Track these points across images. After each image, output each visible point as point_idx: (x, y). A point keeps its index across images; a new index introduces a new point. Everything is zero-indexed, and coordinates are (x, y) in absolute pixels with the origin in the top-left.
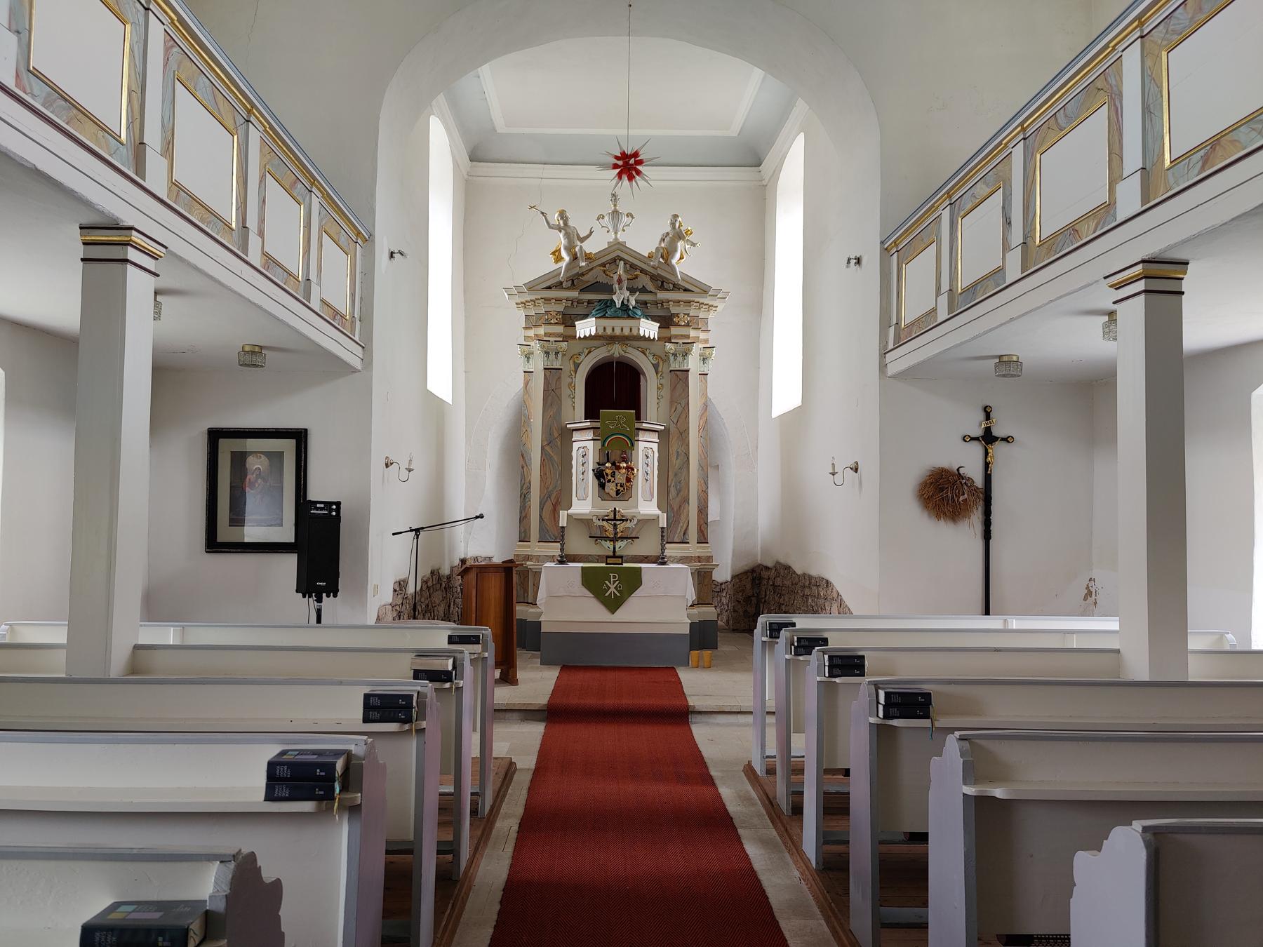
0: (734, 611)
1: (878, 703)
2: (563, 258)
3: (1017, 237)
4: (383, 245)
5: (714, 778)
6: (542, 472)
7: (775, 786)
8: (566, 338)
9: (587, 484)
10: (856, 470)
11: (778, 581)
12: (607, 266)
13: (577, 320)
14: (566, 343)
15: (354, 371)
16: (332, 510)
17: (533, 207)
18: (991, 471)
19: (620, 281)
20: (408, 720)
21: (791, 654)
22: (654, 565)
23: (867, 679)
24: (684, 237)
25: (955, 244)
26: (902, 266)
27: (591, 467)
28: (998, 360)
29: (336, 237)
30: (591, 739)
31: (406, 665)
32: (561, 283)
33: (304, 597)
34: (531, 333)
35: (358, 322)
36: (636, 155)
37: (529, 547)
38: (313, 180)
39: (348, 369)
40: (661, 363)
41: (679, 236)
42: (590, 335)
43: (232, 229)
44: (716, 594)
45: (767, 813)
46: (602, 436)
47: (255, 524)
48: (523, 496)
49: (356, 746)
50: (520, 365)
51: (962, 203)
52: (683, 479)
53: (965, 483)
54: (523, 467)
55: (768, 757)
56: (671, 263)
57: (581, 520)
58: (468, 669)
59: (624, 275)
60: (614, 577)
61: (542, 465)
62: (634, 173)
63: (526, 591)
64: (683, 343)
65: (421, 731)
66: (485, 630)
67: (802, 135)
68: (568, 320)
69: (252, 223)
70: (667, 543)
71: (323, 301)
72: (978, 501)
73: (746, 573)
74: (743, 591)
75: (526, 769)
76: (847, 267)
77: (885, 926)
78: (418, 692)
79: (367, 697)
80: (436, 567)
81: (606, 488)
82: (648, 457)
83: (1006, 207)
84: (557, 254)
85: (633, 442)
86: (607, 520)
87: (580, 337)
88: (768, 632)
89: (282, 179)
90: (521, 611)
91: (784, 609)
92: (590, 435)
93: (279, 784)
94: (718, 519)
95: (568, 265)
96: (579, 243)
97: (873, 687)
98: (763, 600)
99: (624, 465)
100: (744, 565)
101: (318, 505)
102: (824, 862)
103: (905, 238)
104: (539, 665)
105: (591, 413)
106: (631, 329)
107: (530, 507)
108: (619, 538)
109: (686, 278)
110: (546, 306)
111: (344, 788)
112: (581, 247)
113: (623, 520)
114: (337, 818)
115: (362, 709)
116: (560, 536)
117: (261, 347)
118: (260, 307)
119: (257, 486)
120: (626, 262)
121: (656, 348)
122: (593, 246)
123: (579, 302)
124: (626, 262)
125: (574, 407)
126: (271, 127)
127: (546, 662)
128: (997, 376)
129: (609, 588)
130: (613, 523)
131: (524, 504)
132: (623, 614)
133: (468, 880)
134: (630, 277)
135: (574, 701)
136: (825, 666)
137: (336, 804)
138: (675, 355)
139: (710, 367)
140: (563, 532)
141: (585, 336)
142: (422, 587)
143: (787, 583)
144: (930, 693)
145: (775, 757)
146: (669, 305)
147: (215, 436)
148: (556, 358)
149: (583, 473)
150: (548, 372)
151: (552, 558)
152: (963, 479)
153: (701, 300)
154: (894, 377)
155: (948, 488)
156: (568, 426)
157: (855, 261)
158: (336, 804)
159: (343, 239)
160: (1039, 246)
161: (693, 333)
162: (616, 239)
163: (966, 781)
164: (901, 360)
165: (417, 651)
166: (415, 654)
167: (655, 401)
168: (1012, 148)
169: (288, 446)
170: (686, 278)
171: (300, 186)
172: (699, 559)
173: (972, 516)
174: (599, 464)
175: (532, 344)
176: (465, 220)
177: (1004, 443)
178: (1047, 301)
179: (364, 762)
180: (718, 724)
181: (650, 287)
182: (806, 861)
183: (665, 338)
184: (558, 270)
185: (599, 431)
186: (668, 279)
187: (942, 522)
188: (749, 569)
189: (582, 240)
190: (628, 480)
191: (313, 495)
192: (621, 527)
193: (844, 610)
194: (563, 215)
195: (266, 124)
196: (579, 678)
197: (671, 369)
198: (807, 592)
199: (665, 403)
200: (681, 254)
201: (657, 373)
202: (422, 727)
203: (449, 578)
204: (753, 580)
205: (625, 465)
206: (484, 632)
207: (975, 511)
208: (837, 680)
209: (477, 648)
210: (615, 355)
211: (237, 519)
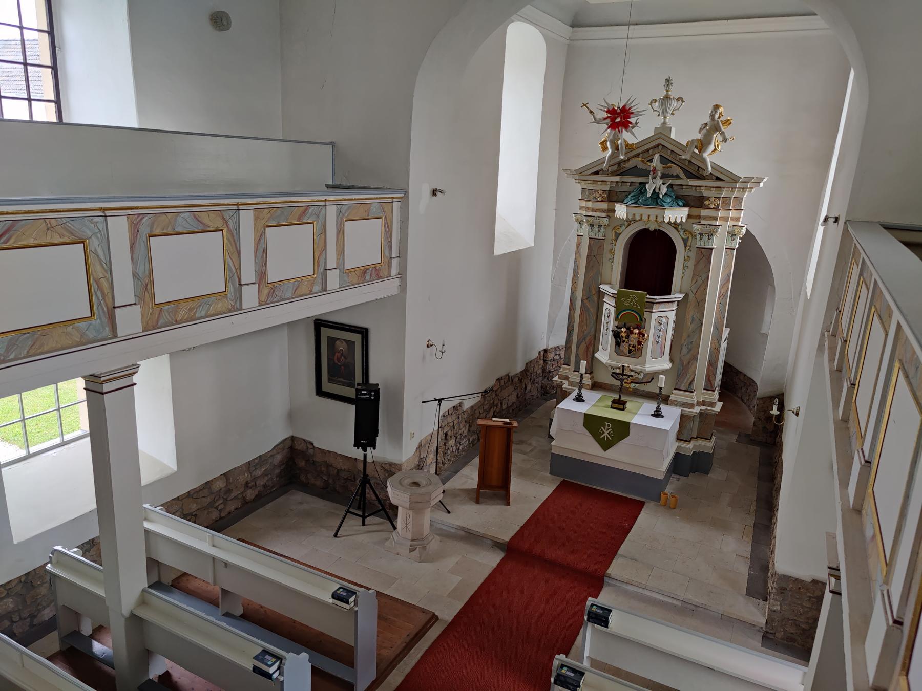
9: (608, 338)
10: (797, 414)
16: (371, 395)
27: (611, 329)
48: (569, 332)
52: (694, 340)
61: (581, 314)
81: (621, 347)
95: (610, 157)
99: (636, 331)
131: (570, 338)
138: (701, 234)
149: (607, 330)
167: (681, 271)
170: (715, 167)
174: (617, 327)
176: (565, 81)
184: (601, 161)
190: (640, 343)
199: (689, 273)
201: (686, 246)
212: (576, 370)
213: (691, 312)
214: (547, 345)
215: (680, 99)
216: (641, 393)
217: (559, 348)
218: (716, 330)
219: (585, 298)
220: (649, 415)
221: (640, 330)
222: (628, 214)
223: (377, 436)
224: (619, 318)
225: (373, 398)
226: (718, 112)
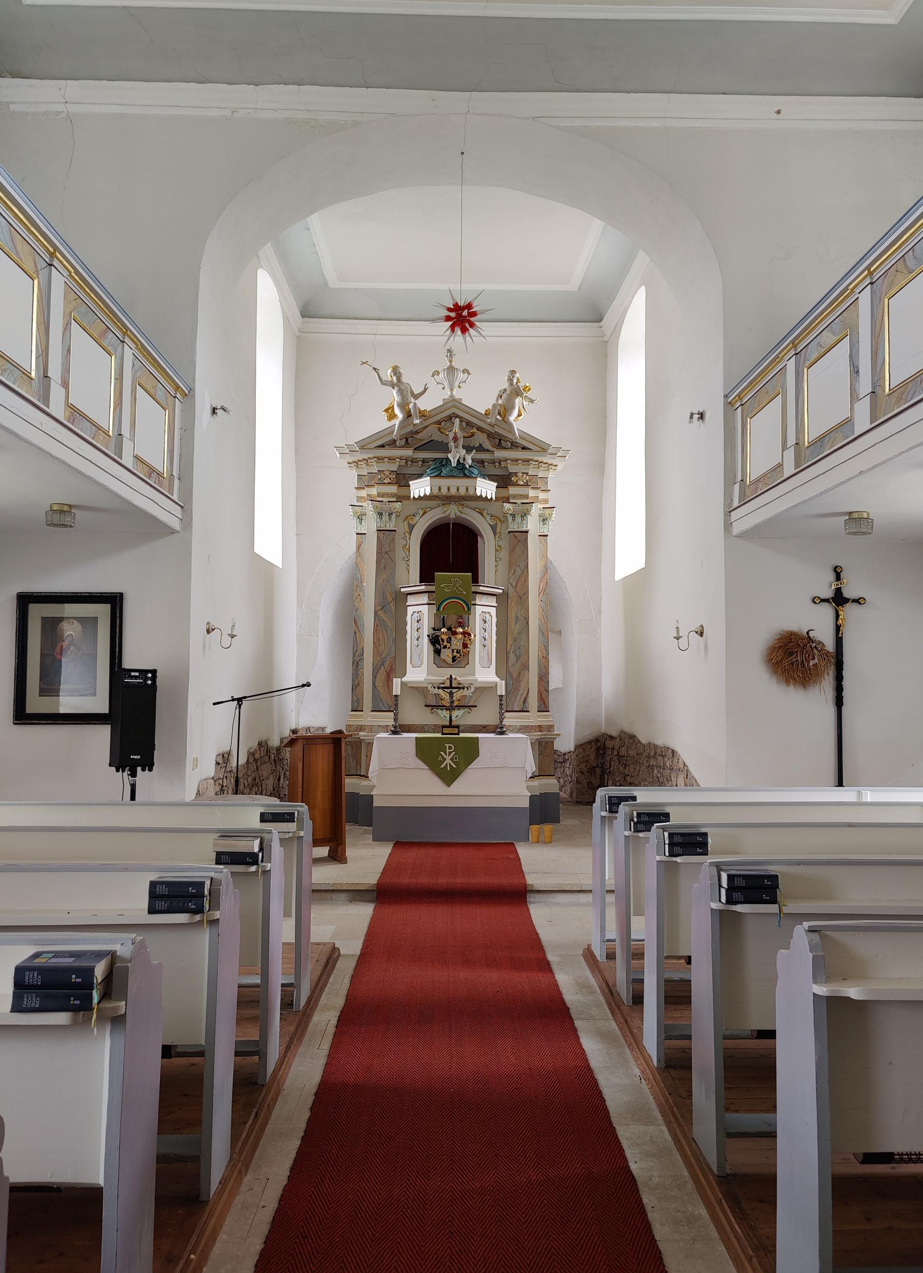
0: (578, 782)
1: (720, 886)
2: (397, 415)
3: (865, 385)
4: (204, 400)
5: (550, 963)
6: (375, 637)
7: (615, 974)
8: (400, 498)
10: (701, 634)
11: (623, 751)
12: (443, 423)
13: (411, 480)
14: (400, 503)
15: (173, 532)
16: (147, 679)
17: (365, 363)
18: (842, 634)
19: (455, 439)
20: (199, 910)
21: (630, 830)
22: (492, 735)
23: (709, 859)
24: (523, 394)
25: (801, 395)
26: (747, 420)
27: (426, 633)
28: (847, 517)
29: (152, 392)
30: (422, 921)
31: (208, 847)
32: (394, 441)
33: (118, 771)
34: (363, 493)
35: (176, 481)
36: (469, 306)
37: (362, 716)
38: (126, 331)
39: (166, 530)
40: (499, 524)
41: (517, 392)
42: (425, 495)
43: (31, 379)
44: (559, 764)
45: (607, 1001)
46: (438, 602)
47: (67, 694)
48: (355, 663)
49: (121, 945)
50: (353, 526)
51: (808, 353)
53: (815, 647)
54: (355, 633)
55: (608, 941)
56: (508, 419)
57: (416, 688)
58: (277, 850)
59: (460, 433)
60: (450, 748)
62: (467, 325)
63: (358, 763)
64: (522, 503)
65: (214, 922)
66: (301, 806)
67: (643, 288)
68: (402, 480)
69: (55, 371)
70: (507, 711)
71: (137, 458)
72: (829, 665)
74: (587, 761)
75: (350, 955)
76: (690, 422)
77: (730, 1135)
78: (212, 879)
79: (153, 885)
80: (264, 738)
83: (854, 355)
84: (390, 411)
85: (469, 606)
86: (443, 688)
87: (414, 497)
88: (607, 806)
89: (90, 328)
90: (350, 784)
91: (629, 780)
92: (424, 599)
93: (28, 993)
94: (561, 686)
95: (401, 423)
96: (413, 400)
97: (714, 869)
98: (608, 771)
100: (588, 734)
101: (133, 674)
102: (666, 1060)
103: (748, 392)
104: (371, 842)
105: (426, 576)
106: (467, 488)
107: (363, 674)
108: (456, 706)
109: (524, 435)
110: (379, 465)
111: (106, 995)
112: (415, 404)
113: (460, 688)
114: (96, 1032)
115: (147, 898)
116: (394, 705)
117: (70, 506)
118: (64, 463)
119: (69, 653)
120: (462, 420)
121: (494, 509)
122: (429, 403)
123: (414, 461)
124: (462, 420)
126: (77, 272)
127: (378, 838)
128: (847, 534)
130: (448, 690)
132: (461, 786)
133: (276, 1084)
134: (466, 435)
135: (405, 880)
136: (665, 844)
137: (95, 1016)
138: (513, 516)
139: (551, 529)
140: (396, 700)
141: (419, 496)
142: (248, 759)
143: (632, 753)
144: (778, 876)
145: (614, 941)
146: (507, 464)
147: (25, 601)
149: (417, 639)
150: (381, 533)
151: (385, 728)
152: (813, 642)
153: (540, 459)
154: (739, 536)
155: (797, 652)
156: (402, 590)
157: (698, 416)
158: (95, 1016)
159: (160, 393)
160: (888, 395)
161: (532, 493)
162: (452, 396)
163: (816, 981)
164: (746, 519)
165: (220, 831)
166: (219, 835)
168: (859, 293)
169: (102, 611)
170: (524, 436)
171: (111, 335)
172: (540, 729)
173: (824, 681)
174: (434, 629)
175: (365, 504)
177: (855, 605)
178: (898, 453)
179: (129, 965)
180: (558, 904)
181: (487, 445)
182: (646, 1058)
183: (503, 498)
184: (390, 430)
185: (434, 595)
186: (506, 437)
187: (791, 688)
188: (593, 738)
189: (416, 397)
190: (465, 646)
191: (128, 663)
192: (458, 695)
193: (691, 782)
194: (396, 371)
195: (70, 268)
196: (412, 855)
197: (510, 530)
198: (652, 762)
199: (503, 565)
200: (519, 411)
201: (495, 534)
202: (216, 918)
203: (278, 749)
204: (598, 750)
205: (461, 630)
206: (299, 809)
207: (826, 676)
208: (679, 859)
209: (292, 826)
211: (50, 687)
212: (373, 710)
213: (514, 610)
215: (465, 371)
216: (463, 728)
218: (541, 633)
221: (464, 628)
223: (155, 750)
224: (441, 610)
225: (149, 682)
226: (516, 376)
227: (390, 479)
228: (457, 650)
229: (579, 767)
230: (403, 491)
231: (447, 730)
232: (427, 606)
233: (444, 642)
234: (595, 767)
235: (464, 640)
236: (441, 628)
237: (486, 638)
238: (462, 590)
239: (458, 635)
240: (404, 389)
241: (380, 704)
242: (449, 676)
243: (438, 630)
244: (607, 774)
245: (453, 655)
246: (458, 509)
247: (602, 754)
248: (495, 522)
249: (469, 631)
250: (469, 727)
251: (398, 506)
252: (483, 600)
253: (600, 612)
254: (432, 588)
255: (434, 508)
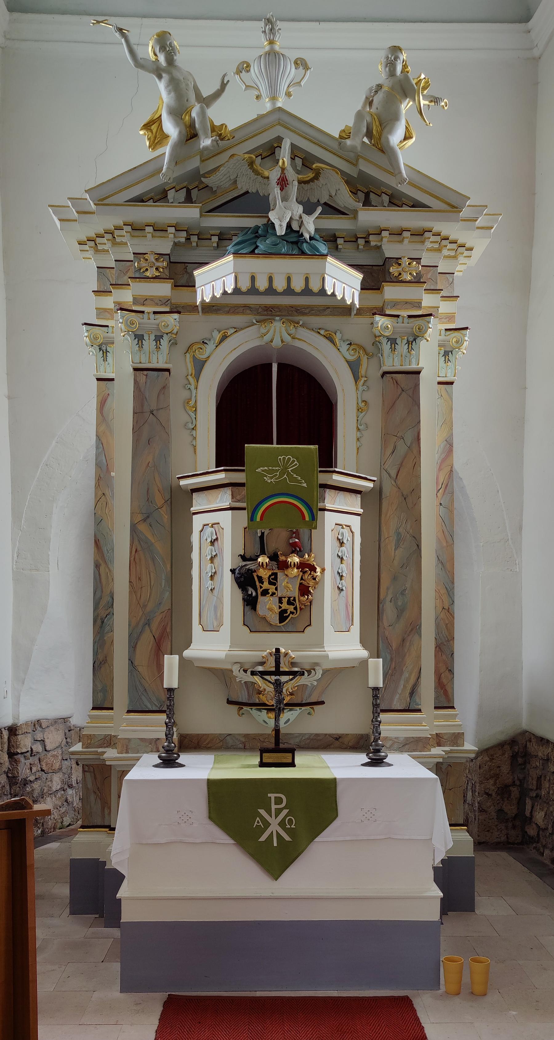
0: (482, 810)
9: (220, 600)
14: (176, 316)
34: (108, 302)
37: (111, 719)
48: (99, 622)
56: (388, 141)
60: (278, 801)
61: (133, 562)
64: (410, 317)
73: (501, 745)
74: (496, 776)
81: (259, 607)
82: (342, 544)
84: (154, 127)
86: (262, 674)
95: (177, 146)
110: (136, 241)
113: (294, 674)
125: (195, 447)
129: (267, 825)
130: (273, 678)
138: (393, 341)
140: (170, 699)
146: (382, 240)
148: (158, 348)
149: (212, 577)
150: (142, 376)
156: (183, 482)
161: (428, 301)
172: (439, 740)
174: (243, 558)
185: (244, 491)
189: (208, 101)
190: (304, 590)
197: (386, 368)
201: (356, 378)
204: (514, 757)
210: (273, 344)
214: (16, 716)
217: (41, 726)
218: (440, 565)
219: (139, 517)
220: (359, 766)
222: (239, 278)
224: (258, 519)
227: (157, 269)
228: (289, 598)
229: (483, 786)
230: (182, 296)
231: (270, 758)
232: (230, 511)
233: (262, 583)
234: (510, 786)
235: (302, 579)
236: (258, 557)
237: (344, 574)
238: (299, 478)
239: (290, 570)
240: (181, 78)
241: (143, 698)
242: (274, 650)
243: (251, 559)
244: (531, 798)
245: (280, 607)
246: (286, 330)
247: (520, 765)
248: (357, 355)
249: (312, 561)
250: (308, 739)
251: (172, 320)
252: (338, 499)
253: (521, 528)
254: (239, 477)
255: (242, 329)
